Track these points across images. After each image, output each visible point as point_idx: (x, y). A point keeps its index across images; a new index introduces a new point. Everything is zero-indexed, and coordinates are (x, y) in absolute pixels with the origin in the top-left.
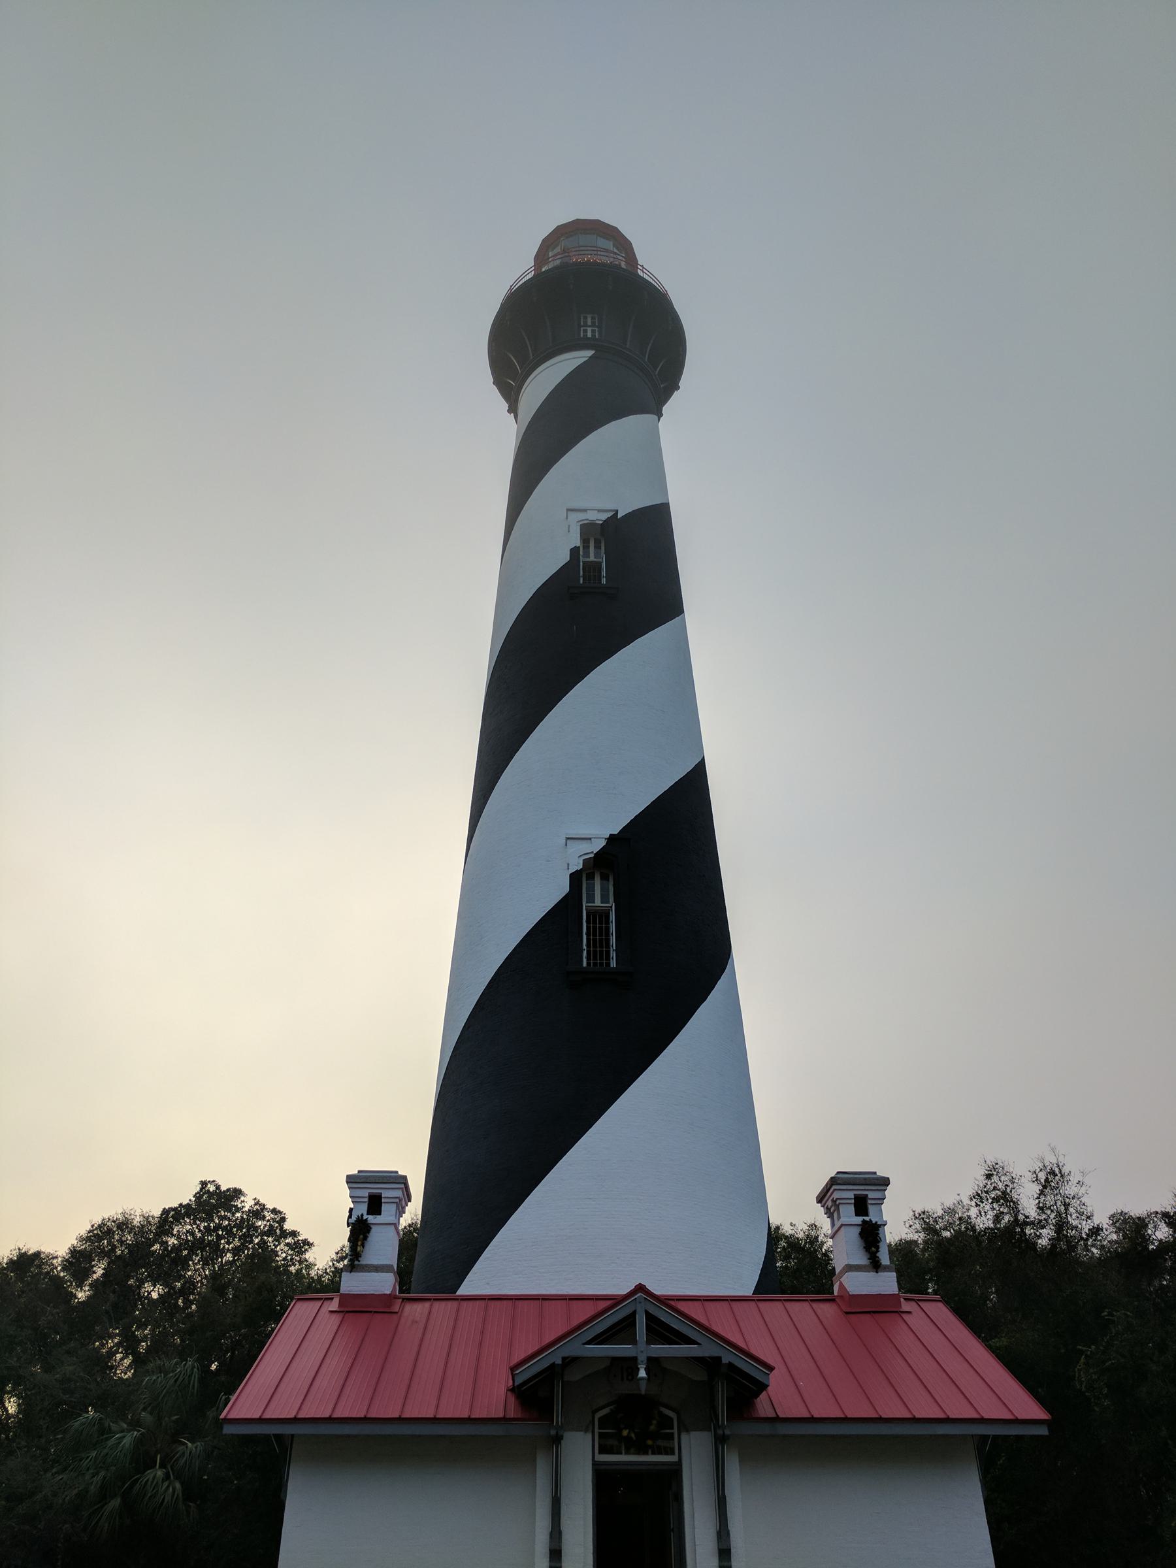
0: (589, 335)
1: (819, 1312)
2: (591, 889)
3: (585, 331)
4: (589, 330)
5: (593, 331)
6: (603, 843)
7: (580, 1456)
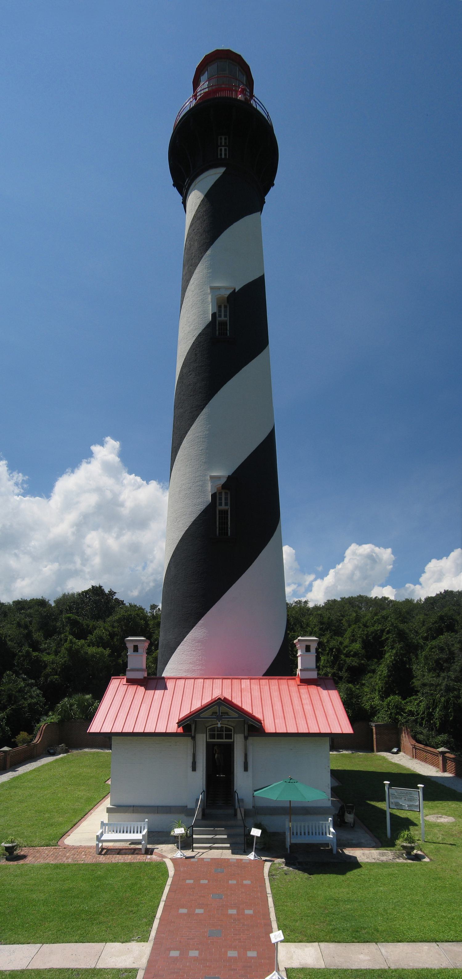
0: (223, 156)
1: (251, 709)
2: (220, 499)
3: (221, 150)
4: (223, 148)
5: (225, 150)
6: (225, 480)
7: (202, 740)
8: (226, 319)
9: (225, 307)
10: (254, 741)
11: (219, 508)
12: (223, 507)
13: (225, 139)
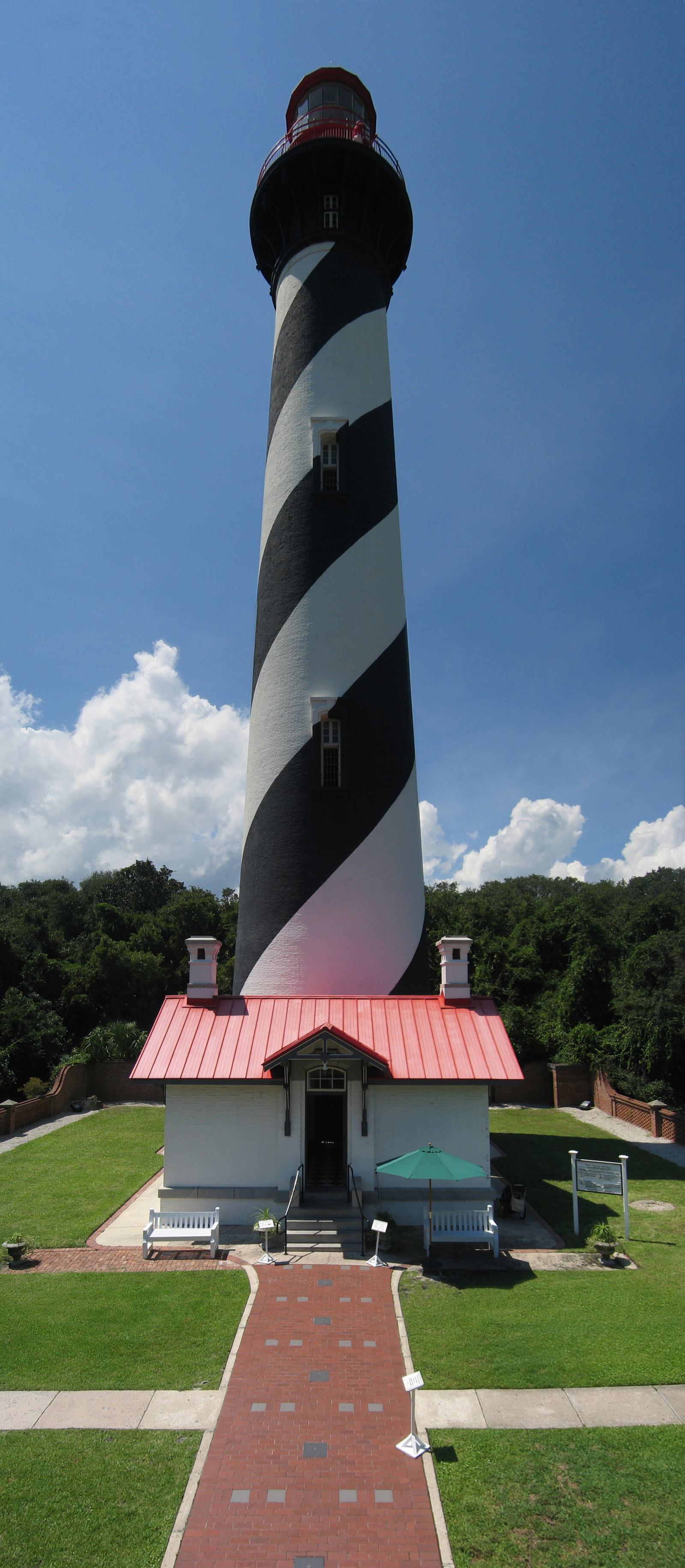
0: (331, 226)
2: (327, 732)
3: (328, 216)
4: (331, 214)
7: (299, 1089)
8: (334, 465)
9: (334, 448)
10: (378, 1094)
11: (324, 745)
12: (331, 744)
13: (334, 200)
